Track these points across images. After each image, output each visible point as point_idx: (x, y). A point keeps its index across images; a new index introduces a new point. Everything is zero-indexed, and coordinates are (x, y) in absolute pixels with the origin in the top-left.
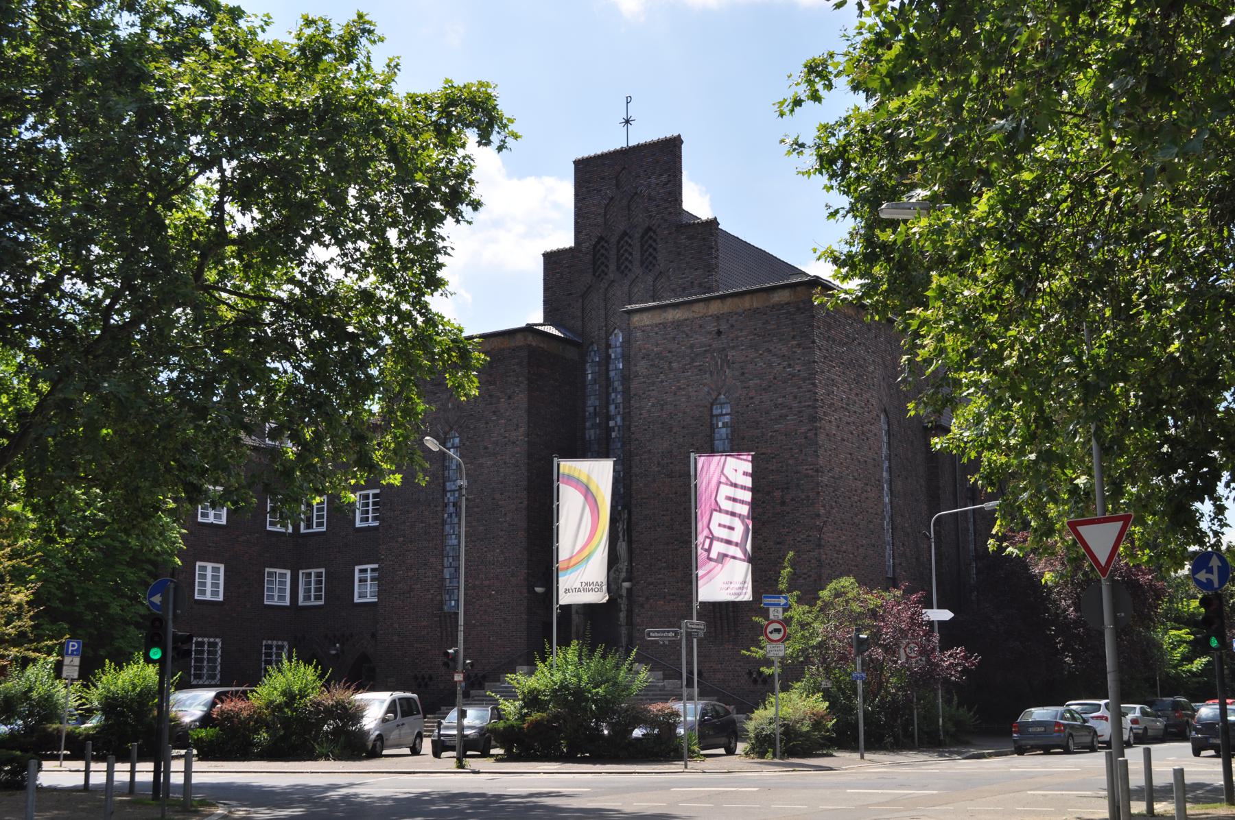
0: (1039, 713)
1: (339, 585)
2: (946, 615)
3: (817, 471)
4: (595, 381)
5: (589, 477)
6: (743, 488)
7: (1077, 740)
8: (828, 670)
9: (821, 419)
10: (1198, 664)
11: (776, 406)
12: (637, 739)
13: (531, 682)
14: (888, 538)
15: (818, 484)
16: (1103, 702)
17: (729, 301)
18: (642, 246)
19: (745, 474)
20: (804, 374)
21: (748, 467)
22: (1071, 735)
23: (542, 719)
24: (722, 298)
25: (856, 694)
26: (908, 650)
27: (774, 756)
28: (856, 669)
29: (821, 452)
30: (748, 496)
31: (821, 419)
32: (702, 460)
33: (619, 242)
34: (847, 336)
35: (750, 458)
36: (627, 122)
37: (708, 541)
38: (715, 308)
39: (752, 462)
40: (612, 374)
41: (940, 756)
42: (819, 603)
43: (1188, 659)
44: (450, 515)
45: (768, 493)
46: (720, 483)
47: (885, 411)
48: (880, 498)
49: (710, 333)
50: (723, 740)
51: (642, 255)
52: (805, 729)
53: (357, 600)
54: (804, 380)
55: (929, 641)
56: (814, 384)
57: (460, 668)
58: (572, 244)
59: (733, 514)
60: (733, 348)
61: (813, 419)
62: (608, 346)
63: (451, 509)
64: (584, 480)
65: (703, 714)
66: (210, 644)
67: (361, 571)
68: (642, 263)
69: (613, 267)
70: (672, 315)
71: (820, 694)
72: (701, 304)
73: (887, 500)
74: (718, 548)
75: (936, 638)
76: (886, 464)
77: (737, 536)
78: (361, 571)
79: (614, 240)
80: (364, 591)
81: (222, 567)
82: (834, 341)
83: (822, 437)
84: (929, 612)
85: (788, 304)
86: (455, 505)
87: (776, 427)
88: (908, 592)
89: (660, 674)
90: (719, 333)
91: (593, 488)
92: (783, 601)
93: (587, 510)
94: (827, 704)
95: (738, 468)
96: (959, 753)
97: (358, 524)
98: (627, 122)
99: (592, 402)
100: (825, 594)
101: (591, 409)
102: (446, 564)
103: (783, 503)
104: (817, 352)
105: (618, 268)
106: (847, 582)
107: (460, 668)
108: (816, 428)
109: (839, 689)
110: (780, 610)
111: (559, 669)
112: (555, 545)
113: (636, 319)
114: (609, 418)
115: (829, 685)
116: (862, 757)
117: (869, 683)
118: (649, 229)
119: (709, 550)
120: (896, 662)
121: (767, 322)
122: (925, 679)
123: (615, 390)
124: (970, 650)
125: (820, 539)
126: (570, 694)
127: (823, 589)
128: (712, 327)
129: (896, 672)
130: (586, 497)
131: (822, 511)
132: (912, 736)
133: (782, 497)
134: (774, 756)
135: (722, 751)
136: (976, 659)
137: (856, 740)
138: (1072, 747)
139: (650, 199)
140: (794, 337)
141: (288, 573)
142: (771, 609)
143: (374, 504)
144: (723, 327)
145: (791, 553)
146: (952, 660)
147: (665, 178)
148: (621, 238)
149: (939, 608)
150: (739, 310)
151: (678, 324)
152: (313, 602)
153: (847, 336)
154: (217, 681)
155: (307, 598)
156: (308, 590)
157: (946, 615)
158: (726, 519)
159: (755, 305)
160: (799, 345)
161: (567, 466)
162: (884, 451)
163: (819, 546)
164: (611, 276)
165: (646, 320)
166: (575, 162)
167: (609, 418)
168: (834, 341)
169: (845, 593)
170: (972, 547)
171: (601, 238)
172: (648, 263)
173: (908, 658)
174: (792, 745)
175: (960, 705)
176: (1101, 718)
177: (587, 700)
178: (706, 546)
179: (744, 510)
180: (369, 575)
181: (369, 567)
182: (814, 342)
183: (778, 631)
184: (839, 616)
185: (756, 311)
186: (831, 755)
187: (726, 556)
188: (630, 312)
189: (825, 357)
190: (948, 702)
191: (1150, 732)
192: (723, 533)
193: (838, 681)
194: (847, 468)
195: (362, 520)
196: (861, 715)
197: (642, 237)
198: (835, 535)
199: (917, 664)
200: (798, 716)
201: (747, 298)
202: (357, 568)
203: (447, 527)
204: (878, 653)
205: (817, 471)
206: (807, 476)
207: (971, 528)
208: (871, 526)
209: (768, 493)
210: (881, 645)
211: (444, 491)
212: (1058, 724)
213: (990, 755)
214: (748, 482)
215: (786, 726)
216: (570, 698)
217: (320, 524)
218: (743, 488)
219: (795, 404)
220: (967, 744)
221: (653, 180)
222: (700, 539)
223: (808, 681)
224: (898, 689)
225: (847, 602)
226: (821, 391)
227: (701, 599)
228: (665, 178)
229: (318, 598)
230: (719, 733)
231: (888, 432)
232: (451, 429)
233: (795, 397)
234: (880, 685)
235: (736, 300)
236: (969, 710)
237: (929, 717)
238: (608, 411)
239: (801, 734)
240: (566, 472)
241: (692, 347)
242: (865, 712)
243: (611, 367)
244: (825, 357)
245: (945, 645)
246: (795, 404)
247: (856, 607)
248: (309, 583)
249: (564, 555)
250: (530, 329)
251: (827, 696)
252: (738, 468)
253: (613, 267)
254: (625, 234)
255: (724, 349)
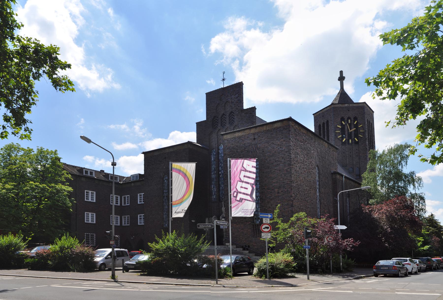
0: (382, 262)
1: (134, 220)
2: (344, 227)
3: (291, 182)
4: (214, 160)
5: (187, 171)
6: (254, 173)
7: (402, 272)
8: (294, 246)
9: (293, 165)
10: (426, 247)
11: (276, 161)
12: (204, 268)
13: (158, 247)
14: (319, 206)
15: (292, 186)
16: (408, 259)
17: (258, 128)
18: (229, 118)
19: (253, 167)
20: (286, 150)
21: (254, 164)
22: (400, 270)
23: (159, 260)
24: (256, 127)
25: (306, 254)
26: (328, 239)
27: (266, 277)
28: (306, 246)
29: (293, 176)
30: (254, 176)
31: (293, 165)
32: (233, 161)
33: (221, 117)
34: (303, 140)
35: (255, 160)
36: (224, 80)
37: (235, 193)
38: (253, 131)
39: (256, 162)
40: (220, 158)
41: (343, 277)
42: (290, 221)
43: (423, 245)
44: (165, 200)
45: (273, 190)
46: (241, 170)
47: (317, 166)
48: (316, 193)
49: (251, 139)
50: (247, 269)
51: (229, 120)
52: (281, 267)
53: (139, 224)
54: (286, 152)
55: (337, 236)
56: (290, 154)
57: (113, 239)
58: (205, 119)
59: (248, 183)
60: (260, 143)
61: (290, 165)
62: (219, 149)
63: (166, 198)
64: (185, 172)
65: (236, 260)
66: (91, 235)
67: (140, 216)
68: (229, 123)
69: (219, 125)
70: (237, 134)
71: (290, 254)
72: (248, 130)
73: (318, 194)
74: (240, 196)
75: (340, 235)
76: (318, 183)
77: (249, 192)
78: (140, 216)
79: (220, 117)
80: (141, 222)
81: (95, 214)
82: (298, 140)
83: (293, 171)
84: (337, 226)
85: (280, 127)
86: (167, 196)
87: (276, 168)
88: (329, 218)
89: (235, 246)
90: (254, 139)
91: (187, 174)
92: (270, 216)
93: (185, 184)
94: (293, 257)
95: (250, 165)
96: (351, 276)
97: (139, 203)
98: (224, 80)
99: (213, 167)
100: (293, 219)
101: (213, 169)
102: (164, 214)
103: (278, 193)
104: (291, 143)
105: (221, 125)
106: (302, 214)
107: (113, 239)
108: (291, 168)
109: (299, 252)
110: (269, 219)
111: (169, 241)
112: (170, 195)
113: (225, 137)
114: (219, 171)
115: (295, 250)
116: (308, 279)
117: (312, 250)
118: (232, 112)
119: (236, 197)
120: (323, 243)
121: (272, 134)
122: (336, 249)
123: (221, 163)
124: (356, 240)
125: (292, 204)
126: (170, 251)
127: (292, 217)
128: (252, 137)
129: (324, 247)
130: (185, 178)
131: (293, 195)
132: (330, 269)
133: (278, 191)
134: (266, 277)
135: (247, 273)
136: (358, 243)
137: (306, 270)
138: (400, 275)
139: (232, 102)
140: (282, 138)
141: (119, 217)
142: (264, 219)
143: (143, 197)
144: (256, 137)
145: (279, 205)
146: (348, 243)
147: (237, 95)
148: (222, 116)
149: (341, 225)
150: (262, 131)
151: (239, 137)
152: (126, 225)
153: (303, 140)
154: (119, 246)
155: (125, 223)
156: (125, 222)
157: (344, 227)
158: (244, 185)
159: (268, 129)
160: (284, 141)
161: (176, 165)
162: (317, 178)
163: (292, 206)
164: (219, 128)
165: (228, 137)
166: (206, 94)
167: (219, 171)
168: (298, 140)
169: (301, 219)
170: (348, 211)
171: (215, 117)
172: (231, 123)
173: (329, 242)
174: (274, 274)
175: (348, 258)
176: (408, 264)
177: (177, 253)
178: (235, 195)
179: (252, 181)
180: (142, 217)
181: (142, 215)
182: (290, 139)
183: (268, 228)
184: (299, 227)
185: (268, 131)
186: (293, 277)
187: (243, 199)
188: (223, 135)
189: (295, 145)
190: (343, 257)
191: (422, 269)
192: (243, 190)
193: (298, 249)
194: (303, 182)
195: (140, 202)
196: (308, 262)
197: (229, 115)
198: (298, 203)
199: (333, 244)
200: (279, 261)
201: (265, 126)
202: (139, 215)
203: (164, 203)
204: (315, 240)
205: (291, 182)
206: (287, 184)
207: (348, 205)
208: (312, 202)
209: (273, 190)
210: (317, 237)
211: (163, 193)
212: (394, 266)
213: (364, 277)
214: (254, 170)
215: (273, 266)
216: (172, 252)
217: (128, 203)
218: (254, 173)
219: (283, 160)
220: (351, 272)
221: (233, 97)
222: (232, 192)
223: (286, 249)
224: (324, 253)
225: (302, 222)
226: (293, 156)
227: (233, 216)
228: (237, 95)
229: (128, 223)
230: (239, 269)
231: (319, 173)
232: (165, 174)
233: (283, 158)
234: (316, 251)
235: (261, 128)
236: (352, 260)
237: (337, 263)
238: (219, 169)
239: (280, 269)
240: (175, 167)
241: (245, 144)
242: (310, 261)
243: (220, 156)
244: (295, 145)
245: (343, 238)
246: (283, 160)
247: (306, 224)
248: (125, 220)
249: (174, 199)
250: (189, 143)
251: (293, 254)
252: (250, 165)
253: (219, 125)
254: (224, 114)
255: (256, 144)
